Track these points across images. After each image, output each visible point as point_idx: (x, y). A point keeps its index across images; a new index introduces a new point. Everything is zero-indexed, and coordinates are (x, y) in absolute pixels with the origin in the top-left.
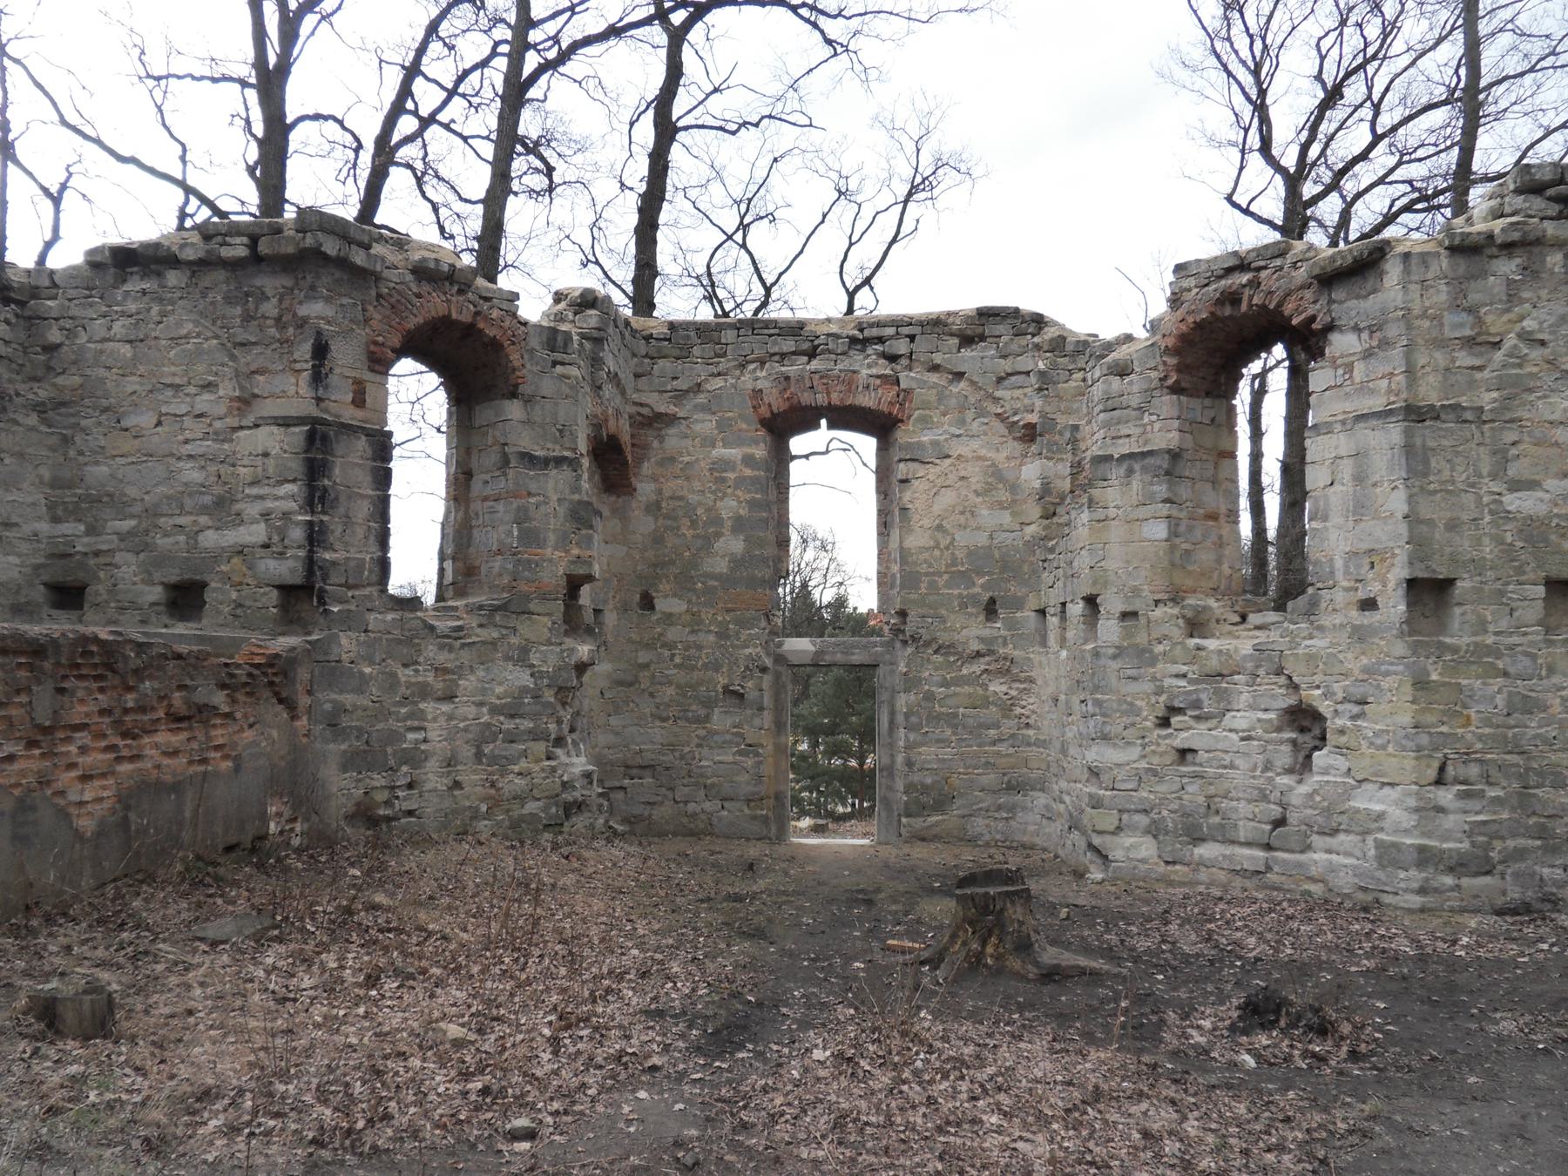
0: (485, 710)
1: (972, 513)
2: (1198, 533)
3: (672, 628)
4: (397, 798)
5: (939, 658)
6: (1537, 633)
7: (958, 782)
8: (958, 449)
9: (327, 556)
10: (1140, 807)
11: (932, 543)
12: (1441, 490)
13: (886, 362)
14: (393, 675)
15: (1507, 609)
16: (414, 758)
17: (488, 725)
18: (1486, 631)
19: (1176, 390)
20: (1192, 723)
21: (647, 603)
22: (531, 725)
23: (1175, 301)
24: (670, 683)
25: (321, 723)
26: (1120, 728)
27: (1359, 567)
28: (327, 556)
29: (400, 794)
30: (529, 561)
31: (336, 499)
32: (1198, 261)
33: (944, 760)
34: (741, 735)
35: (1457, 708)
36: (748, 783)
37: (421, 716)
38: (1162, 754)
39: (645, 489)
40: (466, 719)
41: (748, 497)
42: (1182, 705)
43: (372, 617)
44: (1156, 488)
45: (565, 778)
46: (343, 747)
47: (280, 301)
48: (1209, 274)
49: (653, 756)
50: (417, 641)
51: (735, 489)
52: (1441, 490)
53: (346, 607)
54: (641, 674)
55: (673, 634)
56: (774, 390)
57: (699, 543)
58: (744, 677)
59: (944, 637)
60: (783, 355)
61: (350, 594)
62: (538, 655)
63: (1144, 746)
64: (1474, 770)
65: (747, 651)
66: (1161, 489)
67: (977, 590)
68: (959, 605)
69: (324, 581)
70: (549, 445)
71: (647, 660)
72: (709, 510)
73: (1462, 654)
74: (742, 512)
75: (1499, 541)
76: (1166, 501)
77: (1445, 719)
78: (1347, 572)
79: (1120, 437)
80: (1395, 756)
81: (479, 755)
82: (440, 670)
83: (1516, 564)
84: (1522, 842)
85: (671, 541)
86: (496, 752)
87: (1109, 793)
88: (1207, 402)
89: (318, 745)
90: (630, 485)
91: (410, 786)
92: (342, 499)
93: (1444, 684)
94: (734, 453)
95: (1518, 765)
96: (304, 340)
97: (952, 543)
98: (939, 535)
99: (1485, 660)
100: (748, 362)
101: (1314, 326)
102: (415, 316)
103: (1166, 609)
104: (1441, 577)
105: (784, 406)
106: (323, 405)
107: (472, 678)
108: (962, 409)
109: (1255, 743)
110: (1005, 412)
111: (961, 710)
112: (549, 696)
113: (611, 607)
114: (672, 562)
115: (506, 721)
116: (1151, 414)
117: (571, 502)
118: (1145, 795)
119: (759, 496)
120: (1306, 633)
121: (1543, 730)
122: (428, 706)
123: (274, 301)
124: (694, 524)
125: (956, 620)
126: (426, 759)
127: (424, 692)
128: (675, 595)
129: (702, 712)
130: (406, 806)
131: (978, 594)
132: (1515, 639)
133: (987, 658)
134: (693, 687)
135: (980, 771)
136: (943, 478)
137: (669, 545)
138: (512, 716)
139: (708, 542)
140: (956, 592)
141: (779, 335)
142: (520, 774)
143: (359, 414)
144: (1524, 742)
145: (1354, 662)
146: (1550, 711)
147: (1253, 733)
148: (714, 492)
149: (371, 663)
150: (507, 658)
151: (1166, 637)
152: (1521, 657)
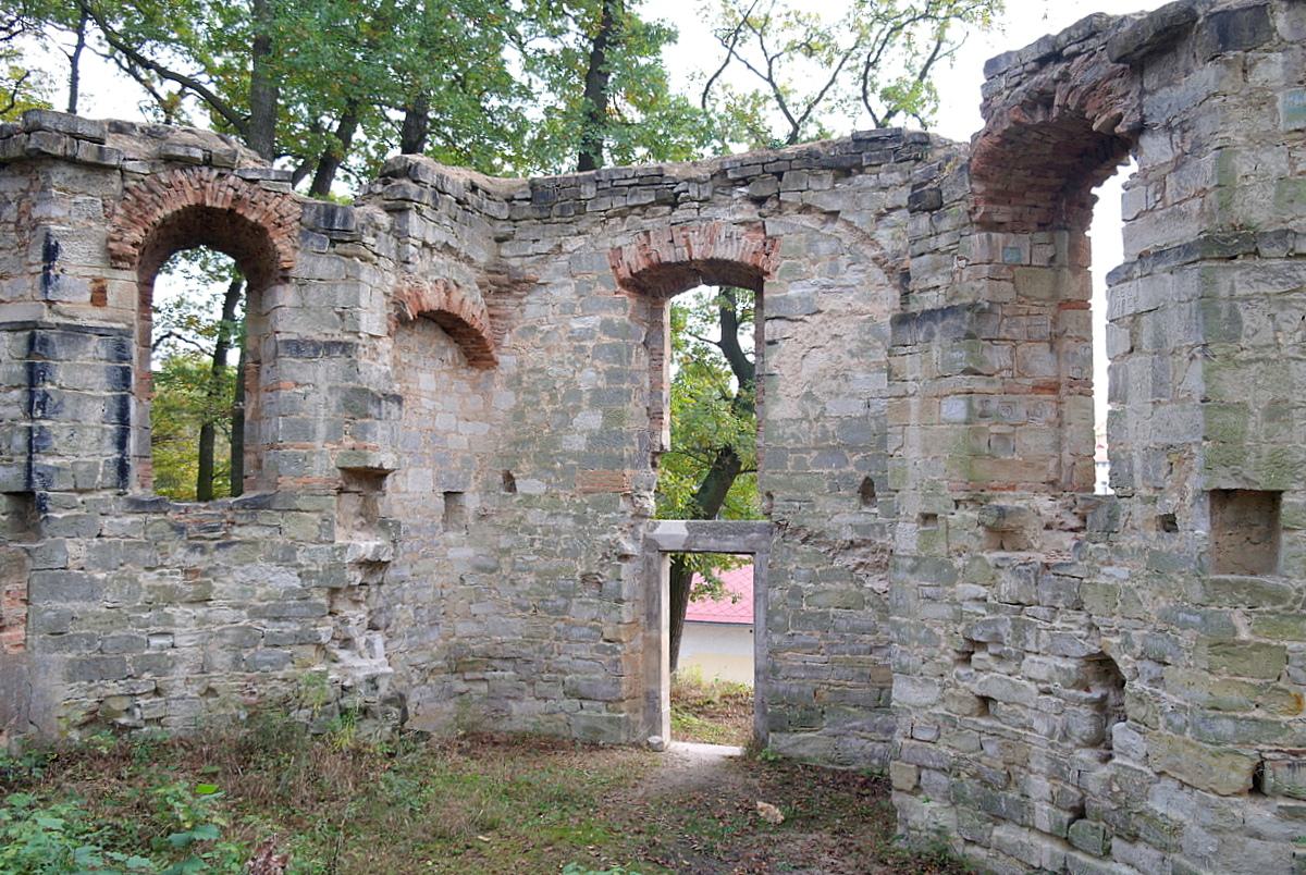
0: (244, 613)
1: (846, 378)
2: (1021, 411)
3: (532, 512)
4: (139, 706)
5: (808, 548)
7: (826, 695)
8: (830, 303)
9: (50, 462)
10: (938, 765)
11: (800, 414)
12: (1258, 360)
13: (753, 207)
14: (134, 580)
16: (160, 665)
17: (247, 629)
19: (988, 225)
20: (992, 663)
21: (509, 482)
22: (298, 628)
23: (986, 109)
24: (530, 570)
25: (40, 632)
26: (919, 660)
27: (1157, 469)
28: (50, 462)
29: (142, 701)
30: (295, 456)
32: (1008, 55)
33: (813, 669)
34: (599, 629)
35: (1281, 684)
36: (606, 683)
37: (169, 619)
38: (962, 700)
39: (507, 361)
40: (222, 623)
41: (606, 366)
42: (981, 639)
44: (956, 355)
45: (347, 684)
47: (19, 204)
48: (1020, 70)
50: (163, 543)
51: (594, 359)
52: (1258, 360)
53: (75, 512)
54: (503, 560)
55: (534, 517)
56: (634, 247)
57: (558, 418)
58: (602, 565)
59: (813, 525)
60: (644, 207)
61: (79, 499)
62: (306, 554)
63: (943, 687)
65: (605, 537)
66: (960, 356)
67: (851, 468)
68: (830, 487)
70: (327, 331)
71: (508, 546)
72: (568, 382)
73: (1289, 603)
74: (600, 384)
76: (966, 371)
77: (1260, 699)
78: (1146, 477)
79: (928, 290)
80: (1193, 746)
81: (237, 661)
85: (531, 417)
86: (258, 657)
87: (907, 742)
88: (1041, 237)
89: (37, 655)
90: (492, 359)
91: (157, 692)
92: (68, 402)
93: (1259, 647)
94: (593, 321)
96: (37, 243)
97: (822, 413)
98: (808, 405)
100: (608, 217)
101: (1119, 129)
102: (161, 208)
103: (965, 512)
104: (1258, 488)
105: (643, 265)
106: (54, 307)
107: (229, 580)
108: (834, 256)
109: (1054, 700)
110: (884, 255)
111: (832, 610)
112: (321, 599)
113: (473, 488)
114: (532, 440)
116: (960, 259)
118: (944, 749)
119: (617, 366)
120: (1103, 558)
122: (178, 612)
123: (14, 204)
124: (553, 398)
125: (826, 504)
126: (173, 665)
127: (171, 596)
128: (534, 475)
129: (561, 602)
131: (852, 474)
133: (863, 550)
134: (553, 574)
135: (854, 683)
136: (812, 337)
137: (529, 421)
138: (277, 619)
139: (566, 416)
140: (826, 471)
141: (638, 185)
142: (284, 680)
143: (98, 312)
145: (1154, 603)
147: (1052, 686)
148: (572, 363)
149: (106, 567)
150: (269, 559)
151: (965, 549)
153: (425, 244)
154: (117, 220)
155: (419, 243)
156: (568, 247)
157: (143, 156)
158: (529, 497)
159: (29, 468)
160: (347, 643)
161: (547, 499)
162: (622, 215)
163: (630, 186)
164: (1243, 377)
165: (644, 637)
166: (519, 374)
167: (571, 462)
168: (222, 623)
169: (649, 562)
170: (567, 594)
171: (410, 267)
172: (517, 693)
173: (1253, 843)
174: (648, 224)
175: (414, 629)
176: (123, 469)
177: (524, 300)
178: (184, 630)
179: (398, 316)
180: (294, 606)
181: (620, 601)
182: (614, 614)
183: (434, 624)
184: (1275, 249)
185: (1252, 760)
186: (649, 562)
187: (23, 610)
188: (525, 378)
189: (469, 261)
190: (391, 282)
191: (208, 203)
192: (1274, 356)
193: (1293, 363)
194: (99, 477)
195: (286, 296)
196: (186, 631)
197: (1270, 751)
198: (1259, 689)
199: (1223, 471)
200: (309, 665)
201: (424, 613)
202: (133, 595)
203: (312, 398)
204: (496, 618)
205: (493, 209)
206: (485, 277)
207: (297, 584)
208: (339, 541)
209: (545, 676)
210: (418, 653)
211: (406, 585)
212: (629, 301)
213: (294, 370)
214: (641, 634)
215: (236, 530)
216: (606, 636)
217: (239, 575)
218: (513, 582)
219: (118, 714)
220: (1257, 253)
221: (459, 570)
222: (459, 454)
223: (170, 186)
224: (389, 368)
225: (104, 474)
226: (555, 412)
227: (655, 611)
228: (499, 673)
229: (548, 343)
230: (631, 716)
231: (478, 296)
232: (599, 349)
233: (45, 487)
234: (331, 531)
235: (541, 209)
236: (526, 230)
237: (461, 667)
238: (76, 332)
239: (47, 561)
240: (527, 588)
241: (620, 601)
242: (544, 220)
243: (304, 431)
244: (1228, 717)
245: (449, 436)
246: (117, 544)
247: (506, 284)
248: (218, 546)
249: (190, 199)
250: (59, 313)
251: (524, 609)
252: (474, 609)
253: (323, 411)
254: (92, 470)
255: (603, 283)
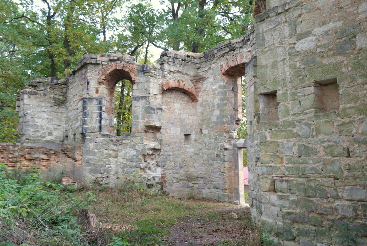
0: (125, 160)
3: (206, 138)
6: (311, 112)
9: (87, 126)
14: (103, 152)
15: (297, 102)
17: (125, 164)
18: (289, 114)
24: (205, 154)
28: (87, 126)
30: (135, 123)
31: (88, 114)
34: (219, 169)
35: (277, 154)
37: (109, 161)
39: (200, 99)
43: (97, 139)
45: (149, 178)
46: (90, 168)
49: (202, 175)
53: (91, 137)
55: (206, 140)
58: (220, 152)
60: (227, 53)
64: (285, 185)
69: (85, 132)
72: (212, 103)
75: (292, 67)
77: (272, 159)
81: (124, 171)
82: (114, 150)
83: (301, 77)
84: (308, 227)
85: (205, 113)
90: (197, 99)
91: (108, 177)
92: (90, 114)
94: (217, 86)
95: (303, 184)
99: (288, 129)
100: (220, 57)
107: (122, 152)
112: (141, 157)
113: (193, 133)
115: (130, 163)
117: (145, 107)
119: (222, 97)
121: (315, 166)
122: (112, 159)
124: (209, 107)
127: (110, 156)
128: (206, 129)
129: (212, 162)
130: (106, 182)
132: (301, 117)
138: (132, 162)
139: (212, 111)
141: (225, 47)
144: (307, 172)
146: (318, 154)
148: (213, 98)
149: (97, 149)
150: (130, 148)
152: (304, 126)
153: (171, 71)
154: (100, 75)
155: (169, 71)
156: (212, 67)
157: (106, 60)
158: (205, 134)
159: (83, 128)
160: (150, 169)
161: (208, 135)
162: (223, 56)
163: (224, 48)
164: (266, 56)
165: (234, 172)
166: (202, 102)
167: (213, 124)
168: (120, 162)
169: (235, 151)
170: (213, 160)
171: (166, 77)
172: (203, 187)
173: (273, 208)
174: (228, 57)
175: (174, 168)
176: (100, 128)
177: (203, 83)
178: (113, 164)
179: (162, 89)
180: (135, 159)
181: (225, 161)
182: (223, 165)
183: (181, 168)
184: (273, 14)
185: (271, 180)
186: (235, 151)
187: (81, 157)
188: (204, 103)
189: (188, 75)
190: (160, 81)
191: (118, 68)
192: (273, 48)
193: (277, 48)
194: (96, 130)
195: (135, 87)
196: (113, 164)
197: (275, 177)
198: (271, 156)
199: (262, 87)
200: (138, 173)
201: (178, 164)
202: (102, 155)
203: (139, 110)
204: (199, 167)
205: (196, 61)
206: (192, 78)
207: (136, 153)
208: (145, 143)
209: (209, 182)
210: (175, 174)
211: (171, 157)
212: (225, 79)
213: (135, 104)
214: (233, 171)
215: (123, 141)
216: (222, 171)
217: (124, 151)
218: (202, 157)
219: (100, 182)
220: (269, 17)
221: (190, 154)
222: (189, 124)
223: (110, 66)
224: (160, 102)
225: (97, 129)
226: (210, 111)
227: (237, 165)
228: (200, 182)
229: (208, 93)
230: (229, 194)
231: (191, 83)
232: (218, 93)
233: (85, 132)
234: (142, 141)
235: (206, 59)
236: (203, 65)
237: (191, 180)
238: (91, 99)
239: (86, 147)
240: (205, 159)
241: (225, 161)
242: (207, 61)
243: (137, 117)
244: (265, 166)
245: (186, 120)
246: (99, 144)
247: (198, 79)
248: (120, 145)
249: (114, 68)
250: (90, 96)
251: (205, 164)
252: (194, 165)
253: (141, 113)
254: (94, 128)
255: (219, 75)
